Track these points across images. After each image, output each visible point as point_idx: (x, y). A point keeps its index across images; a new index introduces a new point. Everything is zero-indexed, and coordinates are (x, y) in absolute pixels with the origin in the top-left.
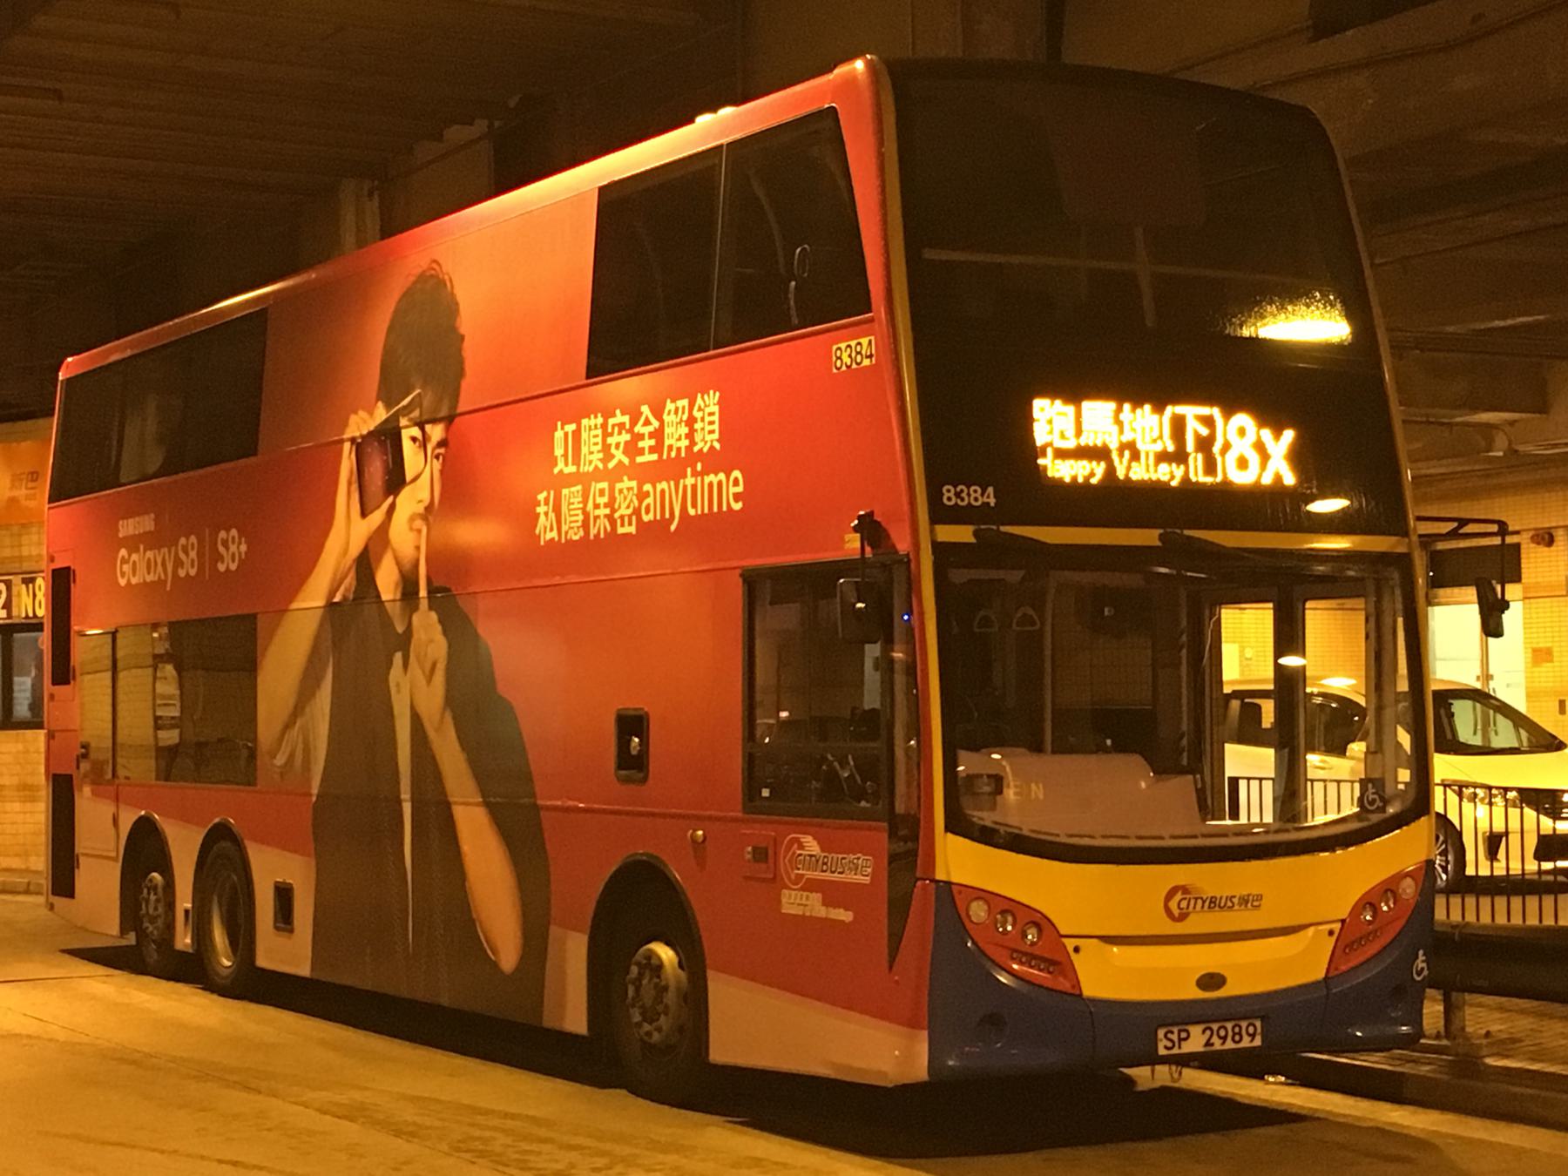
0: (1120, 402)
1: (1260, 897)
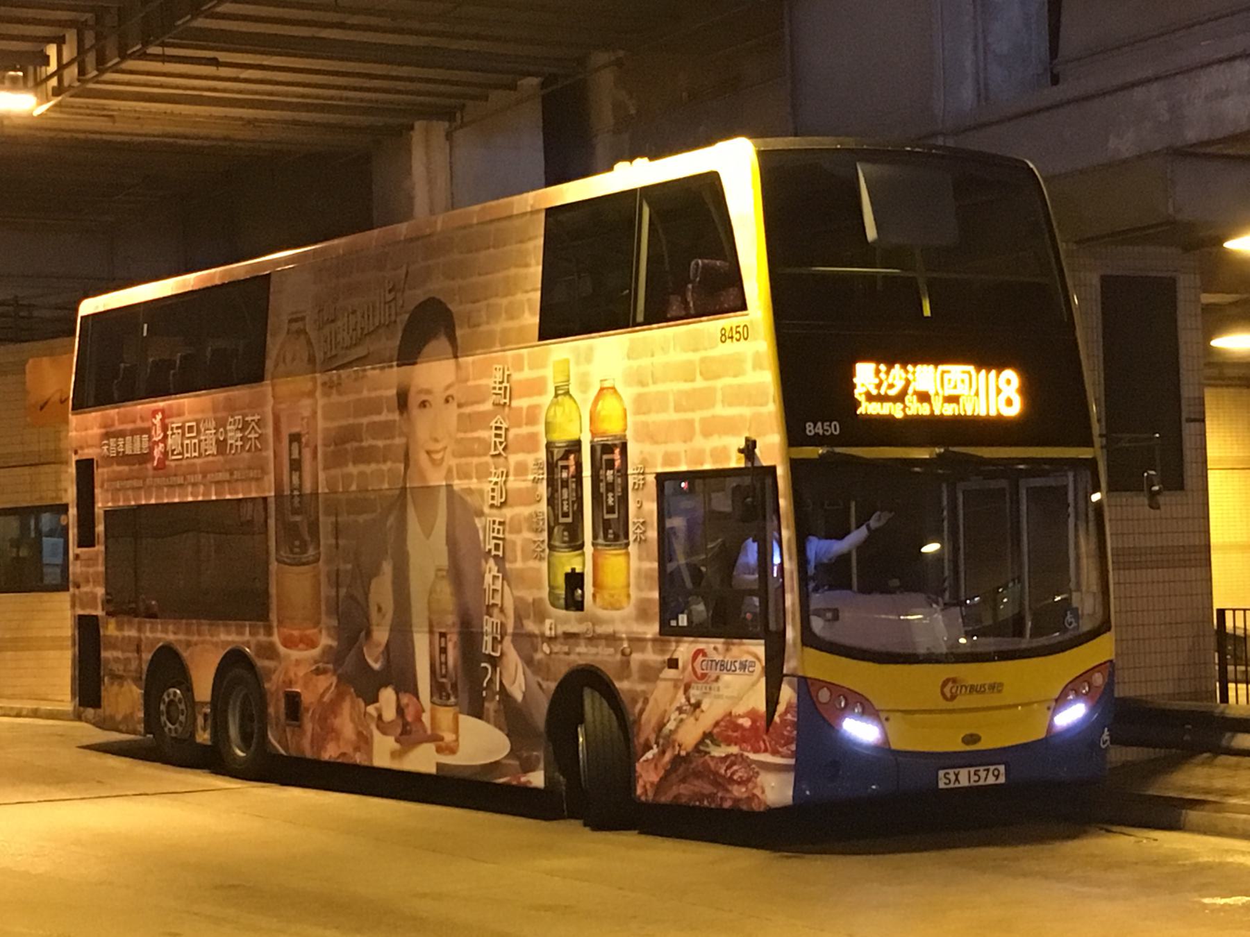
0: (878, 362)
1: (1001, 685)
